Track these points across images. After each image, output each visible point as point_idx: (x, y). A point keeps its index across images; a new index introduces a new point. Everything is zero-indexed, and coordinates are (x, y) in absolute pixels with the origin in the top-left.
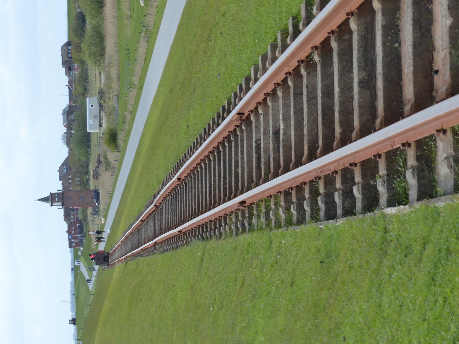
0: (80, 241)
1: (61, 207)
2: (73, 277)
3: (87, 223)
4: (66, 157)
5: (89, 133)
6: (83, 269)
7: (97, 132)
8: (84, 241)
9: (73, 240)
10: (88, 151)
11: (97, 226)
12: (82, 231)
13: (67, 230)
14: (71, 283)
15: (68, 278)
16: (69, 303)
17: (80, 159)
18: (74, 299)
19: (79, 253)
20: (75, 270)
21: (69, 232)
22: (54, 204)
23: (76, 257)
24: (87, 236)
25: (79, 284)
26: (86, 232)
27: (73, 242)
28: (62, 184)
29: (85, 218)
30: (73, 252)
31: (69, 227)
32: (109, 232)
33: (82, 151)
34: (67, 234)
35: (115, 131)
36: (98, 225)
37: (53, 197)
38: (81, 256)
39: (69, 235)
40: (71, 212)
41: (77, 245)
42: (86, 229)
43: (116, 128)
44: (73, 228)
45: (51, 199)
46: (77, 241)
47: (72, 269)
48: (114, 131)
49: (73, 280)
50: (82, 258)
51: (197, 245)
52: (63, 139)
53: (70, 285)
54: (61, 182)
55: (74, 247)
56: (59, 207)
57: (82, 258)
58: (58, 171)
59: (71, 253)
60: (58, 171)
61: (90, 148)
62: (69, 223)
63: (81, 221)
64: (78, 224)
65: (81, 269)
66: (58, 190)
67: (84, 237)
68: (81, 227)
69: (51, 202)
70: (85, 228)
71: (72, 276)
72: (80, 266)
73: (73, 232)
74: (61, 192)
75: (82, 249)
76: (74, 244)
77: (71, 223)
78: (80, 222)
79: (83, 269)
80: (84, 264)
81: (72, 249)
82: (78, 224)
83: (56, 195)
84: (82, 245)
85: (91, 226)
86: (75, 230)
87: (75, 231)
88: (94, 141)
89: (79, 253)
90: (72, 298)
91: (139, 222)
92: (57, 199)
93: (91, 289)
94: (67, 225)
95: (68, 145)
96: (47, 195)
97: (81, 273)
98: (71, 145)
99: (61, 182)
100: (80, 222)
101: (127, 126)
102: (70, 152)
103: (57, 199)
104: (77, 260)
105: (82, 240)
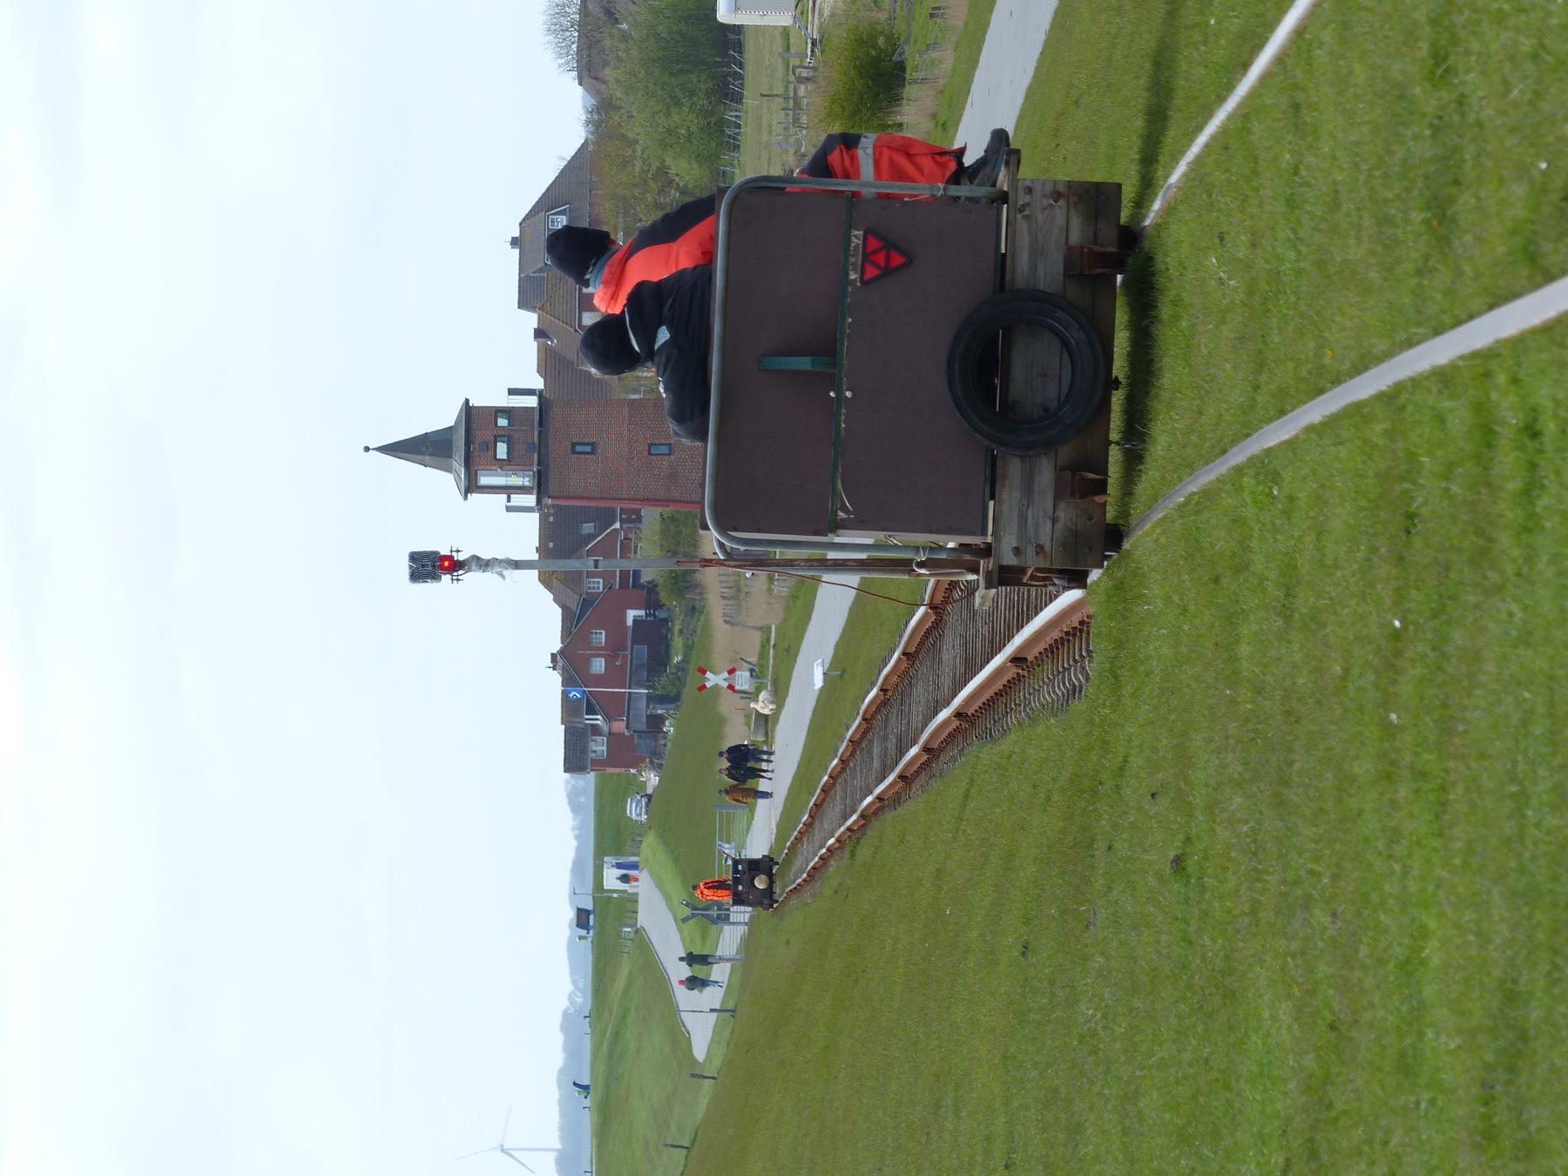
0: (641, 725)
1: (530, 500)
2: (586, 981)
3: (694, 610)
4: (570, 152)
5: (738, 29)
6: (661, 925)
7: (785, 28)
8: (669, 727)
9: (599, 720)
10: (722, 123)
11: (757, 638)
12: (658, 661)
13: (556, 645)
14: (567, 1021)
15: (544, 977)
16: (552, 1156)
17: (663, 171)
18: (587, 1121)
19: (635, 810)
20: (603, 921)
21: (570, 661)
22: (484, 480)
23: (610, 837)
24: (688, 693)
25: (623, 1019)
26: (682, 667)
27: (595, 730)
28: (539, 334)
29: (684, 583)
30: (589, 801)
31: (574, 625)
32: (819, 682)
33: (684, 119)
34: (556, 679)
35: (893, 42)
36: (765, 630)
37: (481, 435)
38: (648, 826)
39: (567, 682)
40: (588, 528)
41: (623, 754)
42: (688, 649)
43: (900, 25)
44: (601, 637)
45: (466, 445)
46: (620, 726)
47: (582, 918)
48: (881, 41)
49: (584, 1000)
50: (650, 842)
51: (982, 754)
52: (555, 28)
53: (559, 1038)
54: (531, 320)
55: (597, 764)
56: (518, 500)
57: (650, 842)
58: (515, 242)
59: (576, 808)
60: (515, 242)
61: (738, 98)
62: (574, 606)
63: (652, 588)
64: (631, 614)
65: (642, 920)
66: (512, 392)
67: (671, 699)
68: (654, 635)
69: (468, 464)
70: (678, 643)
71: (573, 971)
72: (633, 899)
73: (599, 666)
74: (532, 402)
75: (652, 779)
76: (599, 747)
77: (587, 603)
78: (651, 598)
79: (661, 925)
80: (660, 887)
81: (589, 780)
82: (631, 614)
83: (502, 422)
84: (655, 758)
85: (720, 628)
86: (613, 651)
87: (610, 660)
88: (760, 72)
89: (635, 810)
90: (568, 1129)
91: (899, 659)
92: (502, 450)
93: (700, 1051)
94: (556, 612)
95: (589, 68)
96: (445, 417)
97: (642, 942)
98: (608, 73)
99: (531, 320)
100: (651, 598)
101: (946, 58)
102: (604, 116)
103: (502, 450)
104: (618, 852)
105: (655, 723)
